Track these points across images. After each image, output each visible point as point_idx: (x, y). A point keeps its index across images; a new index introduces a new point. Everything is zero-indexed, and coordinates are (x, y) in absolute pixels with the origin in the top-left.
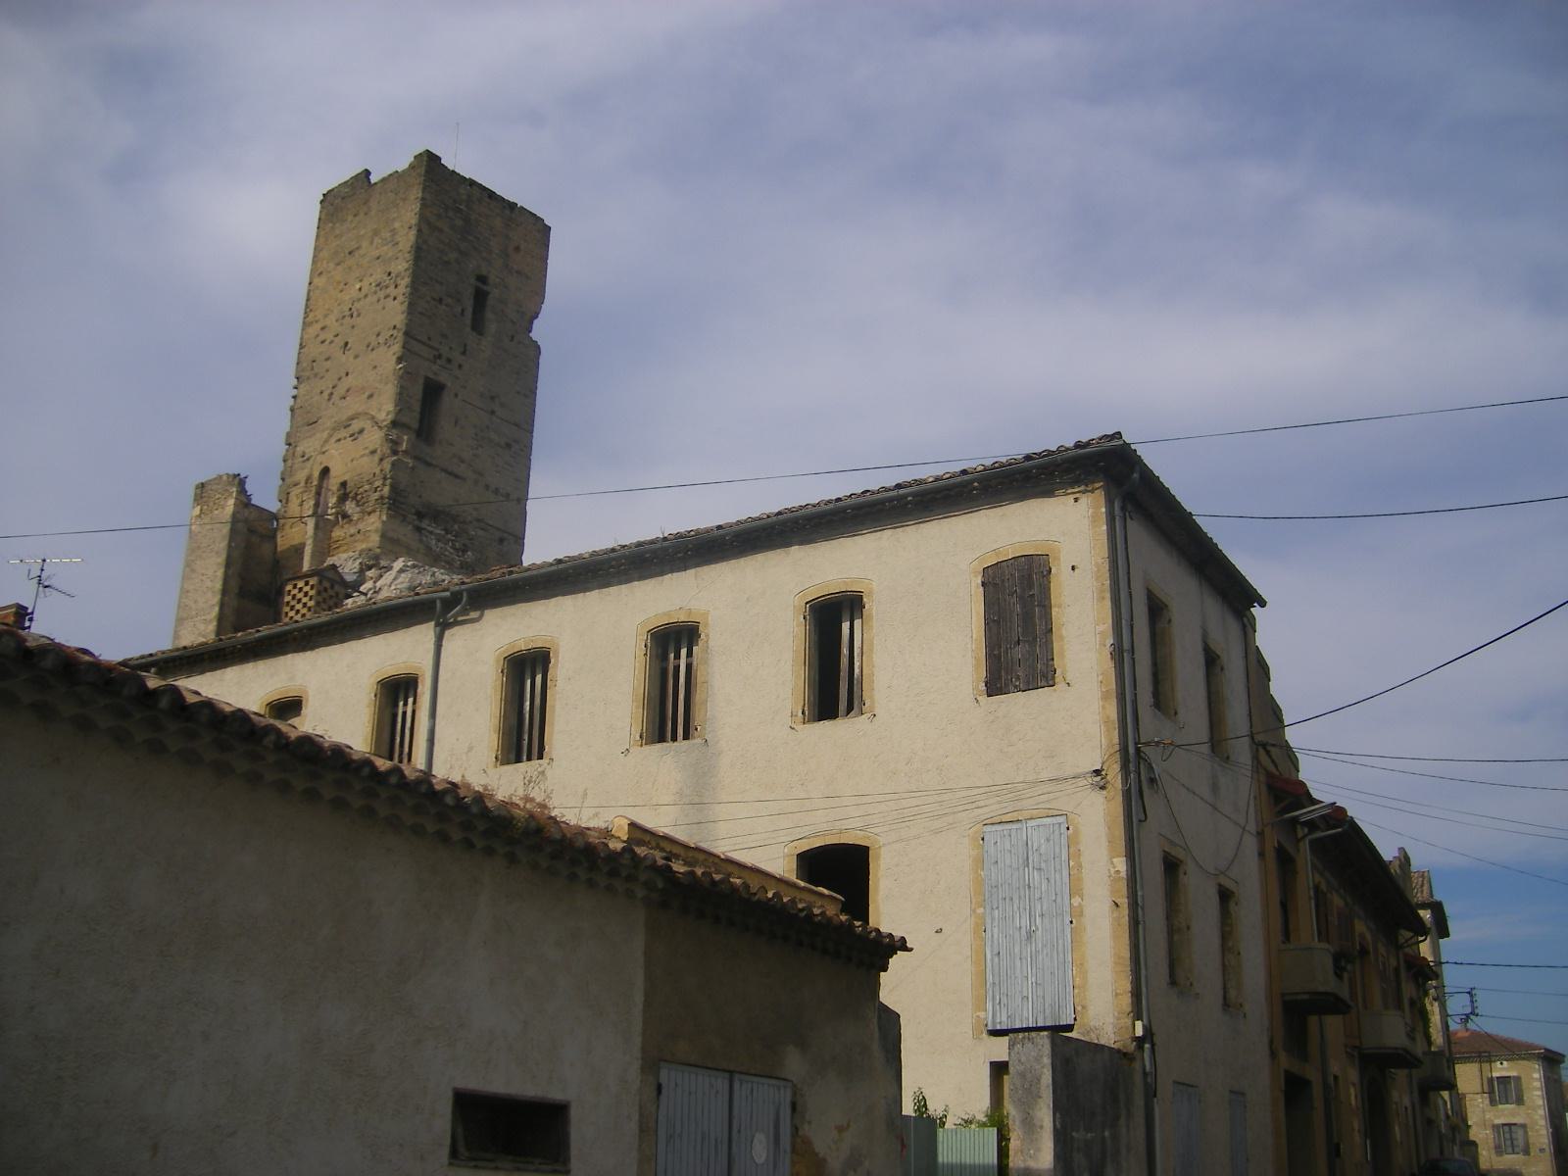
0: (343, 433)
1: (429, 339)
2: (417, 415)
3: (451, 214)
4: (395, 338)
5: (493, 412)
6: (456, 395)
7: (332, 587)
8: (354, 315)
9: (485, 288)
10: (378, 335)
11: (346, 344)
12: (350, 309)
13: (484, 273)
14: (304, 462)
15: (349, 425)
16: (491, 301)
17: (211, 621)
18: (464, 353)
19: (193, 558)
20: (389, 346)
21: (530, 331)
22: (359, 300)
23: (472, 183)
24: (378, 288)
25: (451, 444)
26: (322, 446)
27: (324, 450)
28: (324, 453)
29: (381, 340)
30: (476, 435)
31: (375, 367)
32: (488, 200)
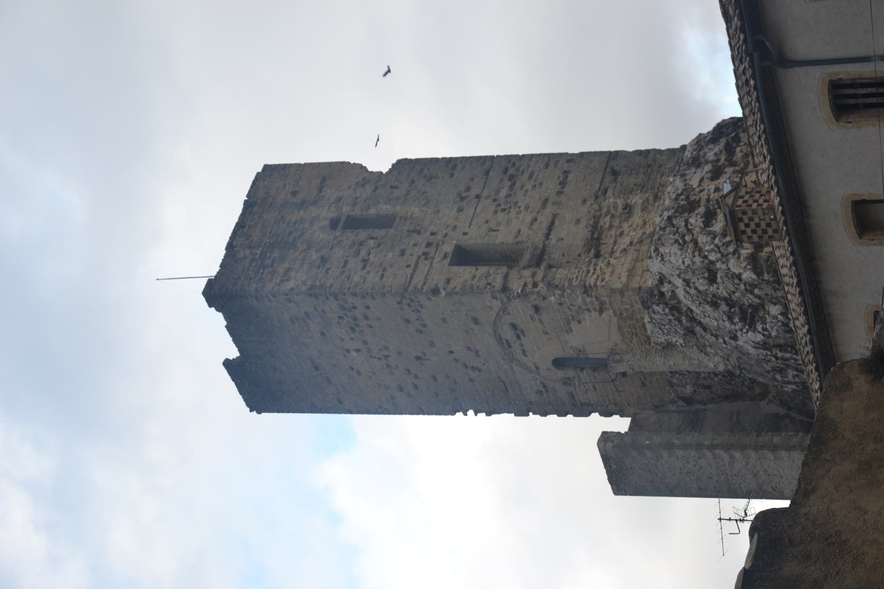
0: (516, 349)
1: (408, 266)
2: (492, 269)
3: (268, 262)
4: (412, 300)
5: (478, 197)
6: (465, 234)
7: (742, 197)
8: (385, 353)
9: (343, 219)
10: (408, 321)
11: (418, 358)
12: (380, 359)
13: (328, 222)
14: (547, 391)
15: (507, 341)
16: (357, 212)
17: (732, 457)
18: (419, 232)
19: (676, 442)
20: (421, 306)
21: (381, 173)
22: (369, 351)
23: (230, 247)
24: (356, 329)
25: (519, 231)
26: (531, 372)
27: (534, 369)
28: (537, 368)
29: (413, 317)
30: (504, 210)
31: (444, 320)
32: (246, 229)
